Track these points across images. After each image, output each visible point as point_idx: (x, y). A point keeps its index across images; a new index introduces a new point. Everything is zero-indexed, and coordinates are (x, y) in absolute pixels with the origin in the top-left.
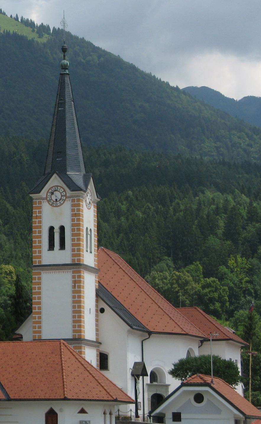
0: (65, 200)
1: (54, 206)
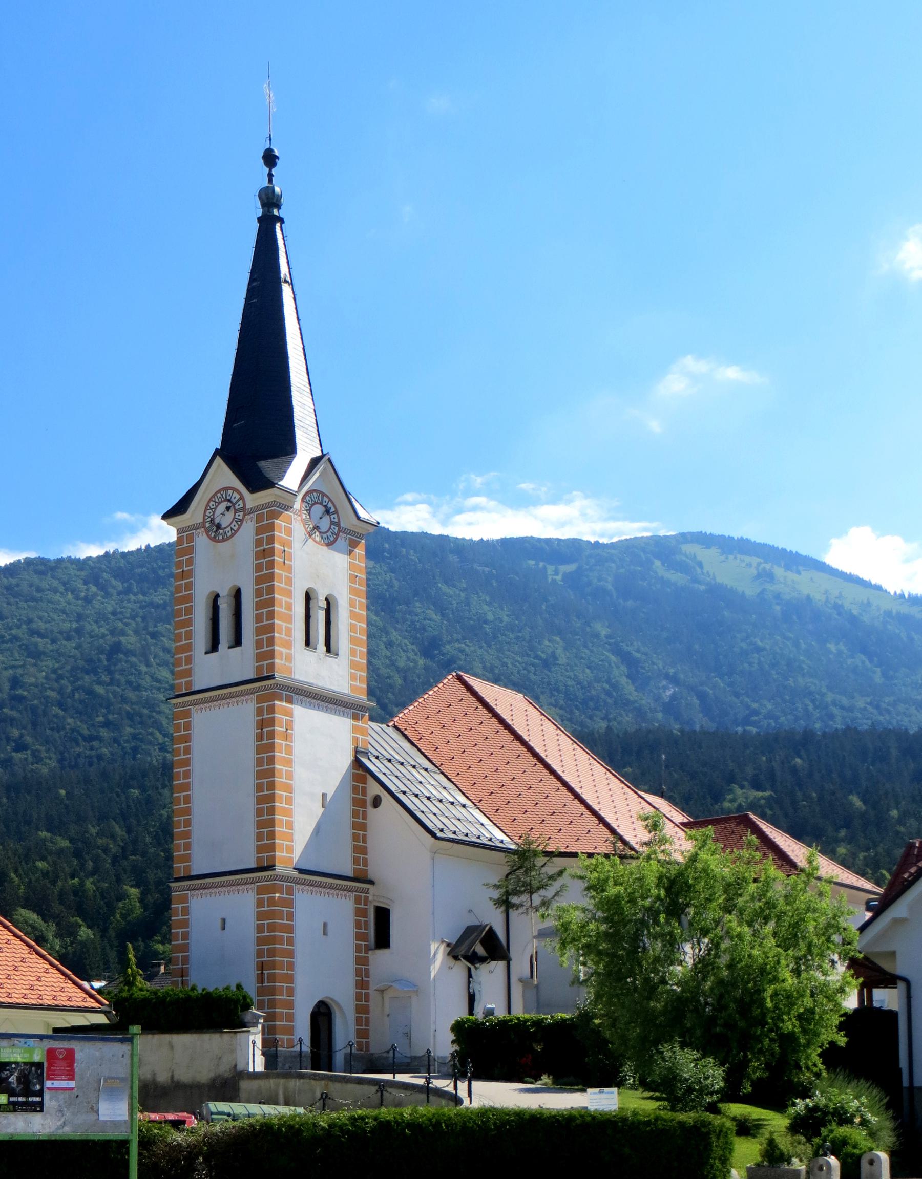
0: (241, 521)
1: (219, 541)
